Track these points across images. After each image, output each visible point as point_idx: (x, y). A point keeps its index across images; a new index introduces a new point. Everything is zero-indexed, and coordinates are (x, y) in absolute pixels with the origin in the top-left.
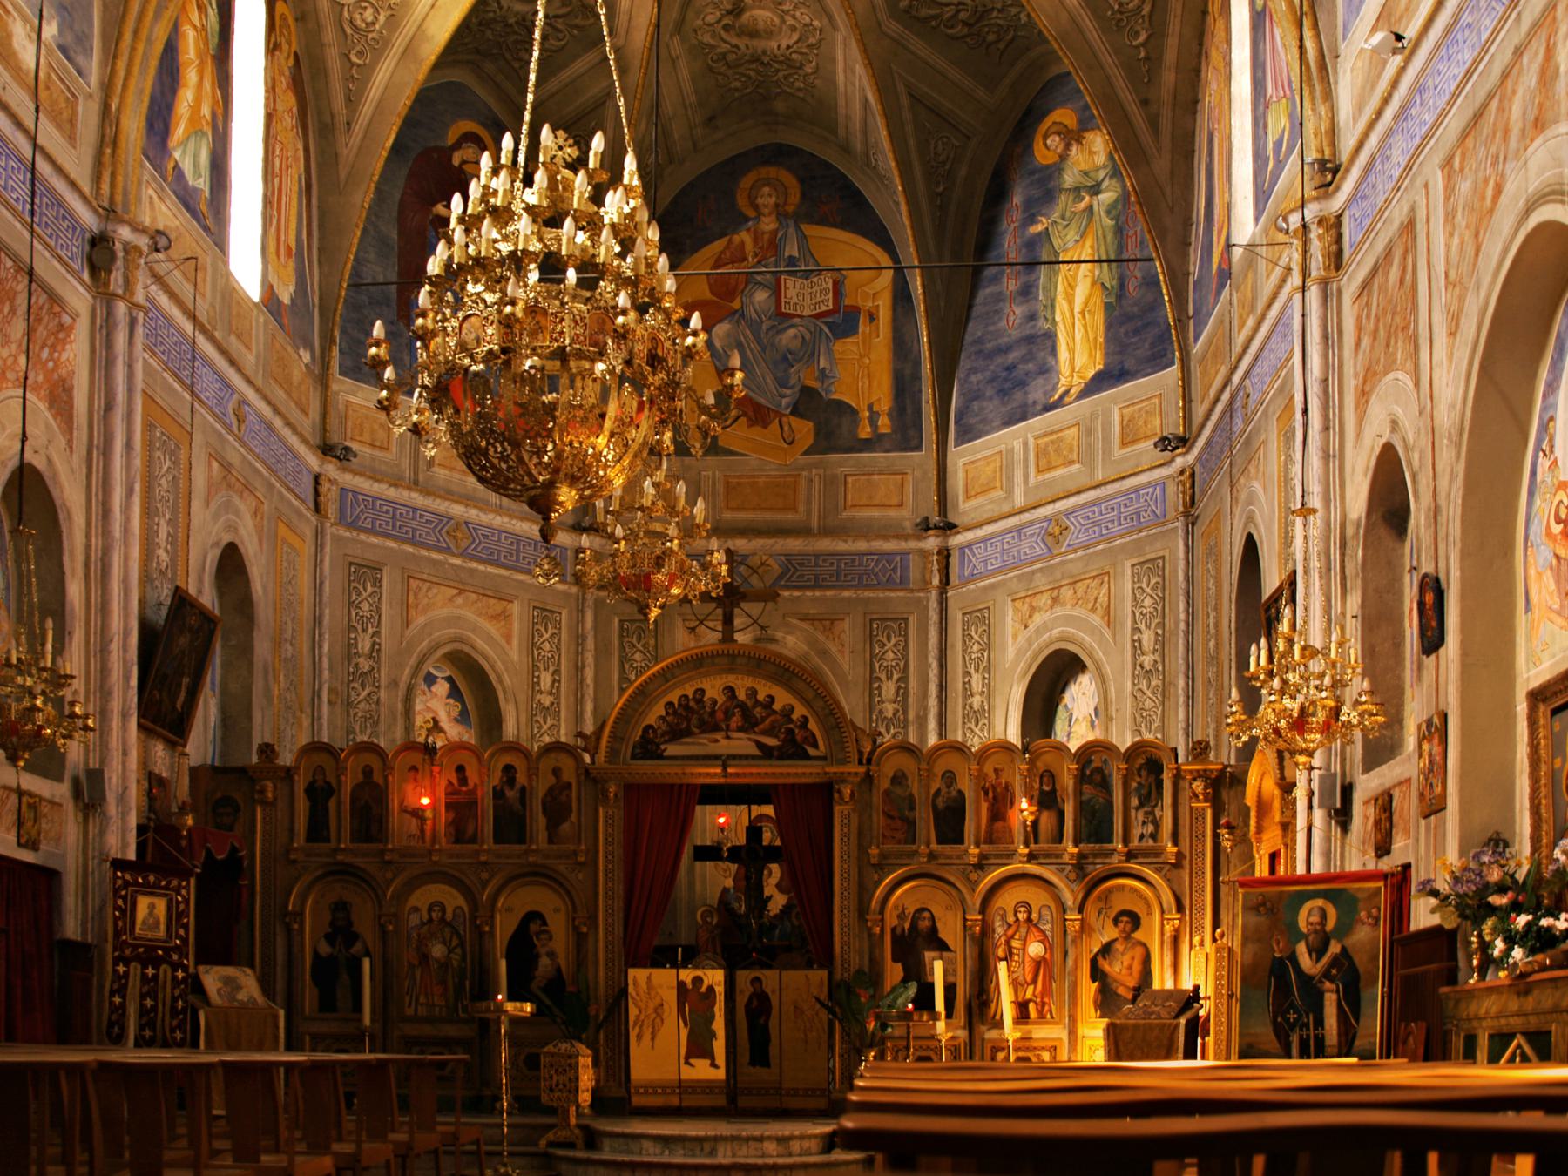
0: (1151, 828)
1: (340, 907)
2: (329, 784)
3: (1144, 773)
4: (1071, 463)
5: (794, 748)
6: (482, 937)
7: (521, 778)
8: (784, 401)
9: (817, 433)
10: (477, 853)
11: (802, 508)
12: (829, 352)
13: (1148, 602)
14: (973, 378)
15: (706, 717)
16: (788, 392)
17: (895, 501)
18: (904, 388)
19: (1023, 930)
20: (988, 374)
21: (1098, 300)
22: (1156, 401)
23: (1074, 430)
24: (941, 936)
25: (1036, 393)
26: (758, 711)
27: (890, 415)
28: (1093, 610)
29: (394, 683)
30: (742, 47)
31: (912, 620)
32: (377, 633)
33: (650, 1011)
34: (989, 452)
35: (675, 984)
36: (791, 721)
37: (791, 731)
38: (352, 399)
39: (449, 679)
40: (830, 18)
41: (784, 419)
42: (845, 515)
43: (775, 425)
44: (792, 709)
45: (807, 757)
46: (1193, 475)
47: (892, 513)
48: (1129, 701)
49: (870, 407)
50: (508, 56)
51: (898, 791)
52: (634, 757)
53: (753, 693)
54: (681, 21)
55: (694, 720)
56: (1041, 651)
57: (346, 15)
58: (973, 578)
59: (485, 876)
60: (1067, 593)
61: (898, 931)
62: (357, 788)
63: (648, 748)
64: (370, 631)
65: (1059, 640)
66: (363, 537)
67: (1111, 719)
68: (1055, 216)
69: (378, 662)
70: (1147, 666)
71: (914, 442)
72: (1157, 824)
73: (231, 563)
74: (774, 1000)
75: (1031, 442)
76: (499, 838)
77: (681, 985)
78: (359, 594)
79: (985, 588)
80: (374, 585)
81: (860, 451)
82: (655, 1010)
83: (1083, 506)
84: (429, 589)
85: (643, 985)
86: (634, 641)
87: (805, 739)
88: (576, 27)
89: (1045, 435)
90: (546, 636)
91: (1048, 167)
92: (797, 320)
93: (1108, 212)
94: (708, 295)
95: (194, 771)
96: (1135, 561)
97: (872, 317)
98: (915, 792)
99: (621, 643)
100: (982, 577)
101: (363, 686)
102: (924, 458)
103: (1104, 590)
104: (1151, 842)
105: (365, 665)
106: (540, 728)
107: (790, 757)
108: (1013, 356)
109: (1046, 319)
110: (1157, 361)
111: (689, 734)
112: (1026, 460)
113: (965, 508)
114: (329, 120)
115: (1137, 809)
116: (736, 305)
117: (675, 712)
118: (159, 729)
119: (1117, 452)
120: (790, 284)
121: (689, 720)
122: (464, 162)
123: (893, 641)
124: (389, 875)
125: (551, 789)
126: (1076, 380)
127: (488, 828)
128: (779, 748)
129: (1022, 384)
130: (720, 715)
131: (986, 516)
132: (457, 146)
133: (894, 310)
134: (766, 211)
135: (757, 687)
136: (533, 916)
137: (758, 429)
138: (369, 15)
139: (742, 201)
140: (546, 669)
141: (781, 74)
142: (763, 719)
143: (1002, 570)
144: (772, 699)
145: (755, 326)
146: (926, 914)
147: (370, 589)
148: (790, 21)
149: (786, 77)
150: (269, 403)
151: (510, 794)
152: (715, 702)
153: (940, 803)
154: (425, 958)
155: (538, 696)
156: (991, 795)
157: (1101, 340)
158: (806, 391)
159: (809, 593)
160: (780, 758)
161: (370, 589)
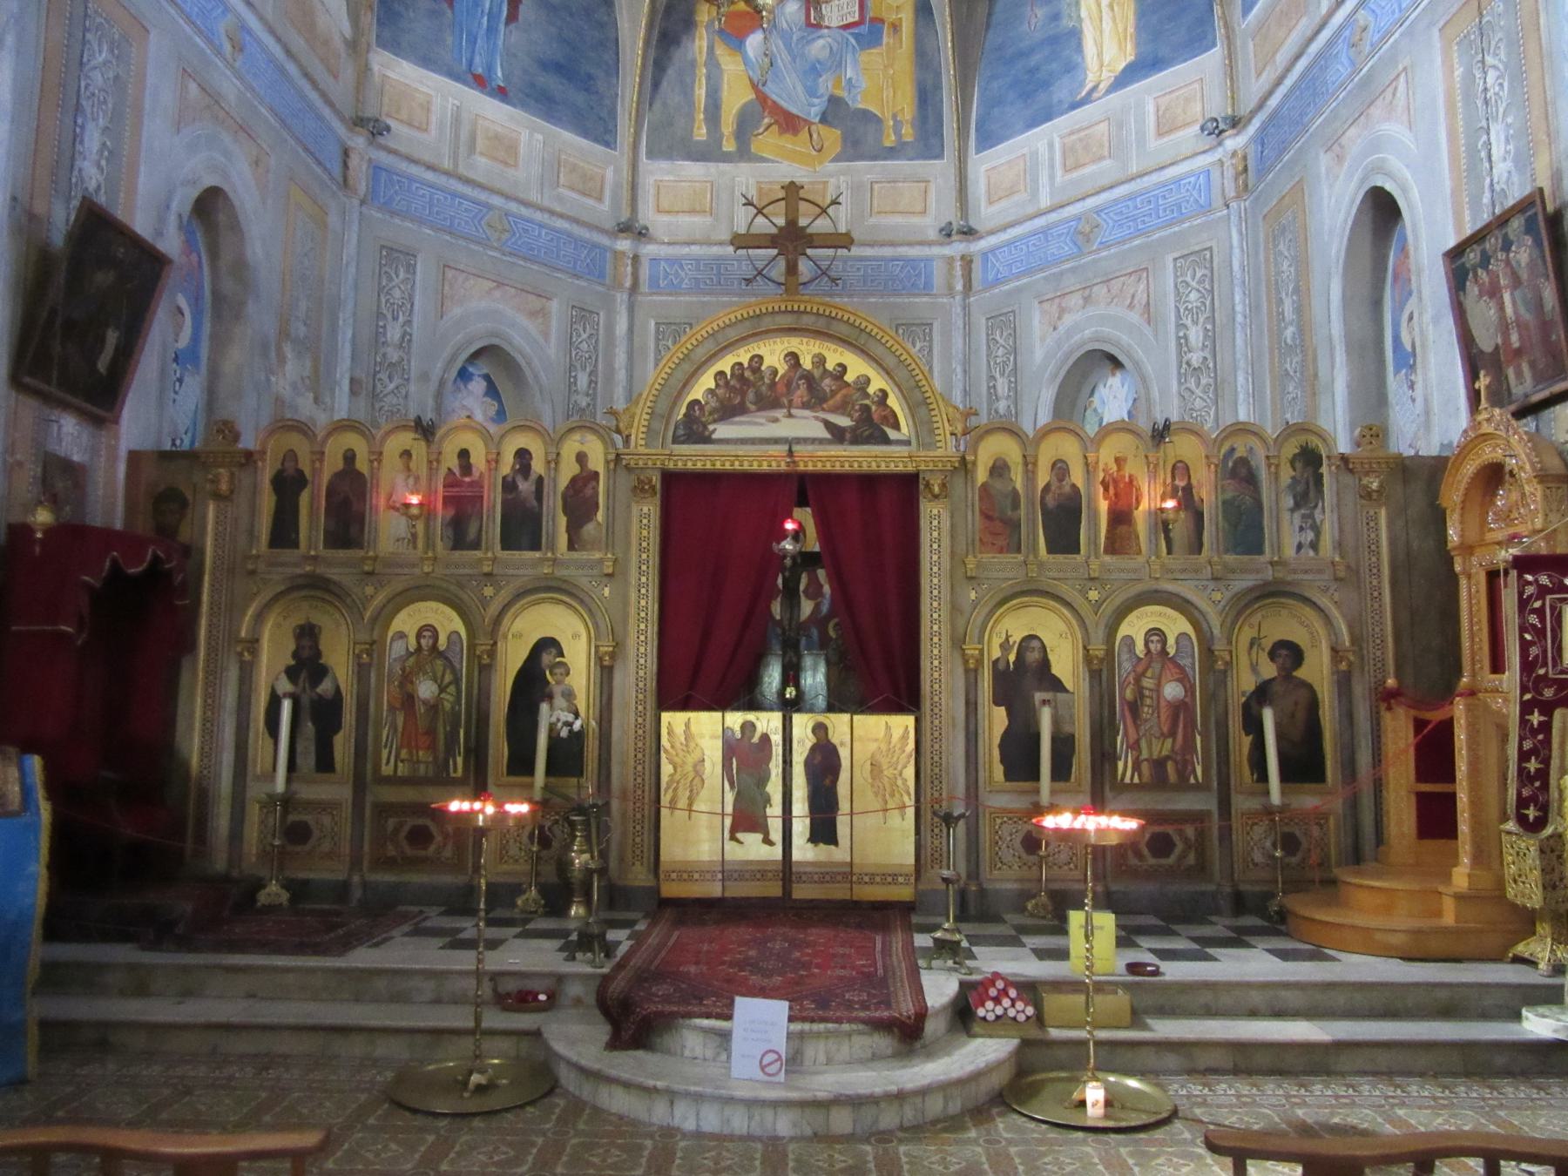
0: (1310, 535)
1: (308, 634)
2: (301, 473)
3: (1298, 465)
4: (1102, 158)
6: (485, 668)
7: (538, 466)
8: (814, 110)
9: (845, 139)
10: (480, 561)
13: (1193, 296)
14: (995, 85)
16: (816, 101)
17: (919, 208)
18: (926, 98)
19: (1157, 666)
22: (1197, 86)
23: (1103, 127)
25: (1060, 92)
26: (827, 384)
27: (913, 125)
28: (1131, 306)
29: (425, 377)
31: (936, 326)
32: (409, 322)
33: (689, 768)
36: (867, 396)
37: (866, 409)
39: (487, 378)
41: (813, 128)
42: (873, 220)
43: (804, 134)
44: (868, 381)
45: (886, 441)
46: (1245, 158)
47: (915, 220)
49: (894, 117)
51: (998, 485)
52: (675, 441)
53: (820, 360)
55: (751, 395)
56: (1071, 352)
58: (998, 282)
59: (488, 591)
60: (1100, 291)
61: (1001, 666)
62: (338, 476)
63: (694, 430)
64: (401, 319)
65: (1091, 340)
69: (408, 353)
70: (1195, 364)
73: (210, 207)
74: (844, 753)
76: (508, 543)
78: (390, 279)
79: (1009, 294)
80: (407, 271)
81: (885, 159)
82: (695, 766)
83: (1116, 201)
84: (467, 279)
85: (679, 729)
87: (885, 419)
89: (1072, 133)
90: (584, 336)
95: (134, 457)
96: (1176, 255)
97: (896, 27)
98: (1019, 486)
99: (657, 346)
100: (1005, 281)
101: (390, 378)
102: (940, 171)
103: (1142, 286)
104: (1311, 553)
105: (394, 355)
108: (1035, 59)
109: (1070, 17)
110: (1197, 41)
111: (741, 410)
112: (1052, 159)
113: (985, 213)
115: (1292, 510)
117: (727, 383)
118: (69, 398)
119: (1153, 143)
121: (743, 394)
123: (918, 345)
124: (369, 590)
125: (574, 480)
126: (1105, 74)
127: (495, 530)
128: (853, 429)
129: (1046, 84)
130: (781, 389)
133: (916, 22)
136: (547, 645)
137: (788, 136)
142: (834, 393)
143: (1028, 272)
145: (786, 37)
146: (1035, 644)
147: (402, 275)
150: (278, 40)
151: (525, 487)
152: (775, 372)
153: (1051, 502)
154: (409, 700)
156: (1112, 491)
157: (1131, 30)
158: (834, 101)
160: (856, 441)
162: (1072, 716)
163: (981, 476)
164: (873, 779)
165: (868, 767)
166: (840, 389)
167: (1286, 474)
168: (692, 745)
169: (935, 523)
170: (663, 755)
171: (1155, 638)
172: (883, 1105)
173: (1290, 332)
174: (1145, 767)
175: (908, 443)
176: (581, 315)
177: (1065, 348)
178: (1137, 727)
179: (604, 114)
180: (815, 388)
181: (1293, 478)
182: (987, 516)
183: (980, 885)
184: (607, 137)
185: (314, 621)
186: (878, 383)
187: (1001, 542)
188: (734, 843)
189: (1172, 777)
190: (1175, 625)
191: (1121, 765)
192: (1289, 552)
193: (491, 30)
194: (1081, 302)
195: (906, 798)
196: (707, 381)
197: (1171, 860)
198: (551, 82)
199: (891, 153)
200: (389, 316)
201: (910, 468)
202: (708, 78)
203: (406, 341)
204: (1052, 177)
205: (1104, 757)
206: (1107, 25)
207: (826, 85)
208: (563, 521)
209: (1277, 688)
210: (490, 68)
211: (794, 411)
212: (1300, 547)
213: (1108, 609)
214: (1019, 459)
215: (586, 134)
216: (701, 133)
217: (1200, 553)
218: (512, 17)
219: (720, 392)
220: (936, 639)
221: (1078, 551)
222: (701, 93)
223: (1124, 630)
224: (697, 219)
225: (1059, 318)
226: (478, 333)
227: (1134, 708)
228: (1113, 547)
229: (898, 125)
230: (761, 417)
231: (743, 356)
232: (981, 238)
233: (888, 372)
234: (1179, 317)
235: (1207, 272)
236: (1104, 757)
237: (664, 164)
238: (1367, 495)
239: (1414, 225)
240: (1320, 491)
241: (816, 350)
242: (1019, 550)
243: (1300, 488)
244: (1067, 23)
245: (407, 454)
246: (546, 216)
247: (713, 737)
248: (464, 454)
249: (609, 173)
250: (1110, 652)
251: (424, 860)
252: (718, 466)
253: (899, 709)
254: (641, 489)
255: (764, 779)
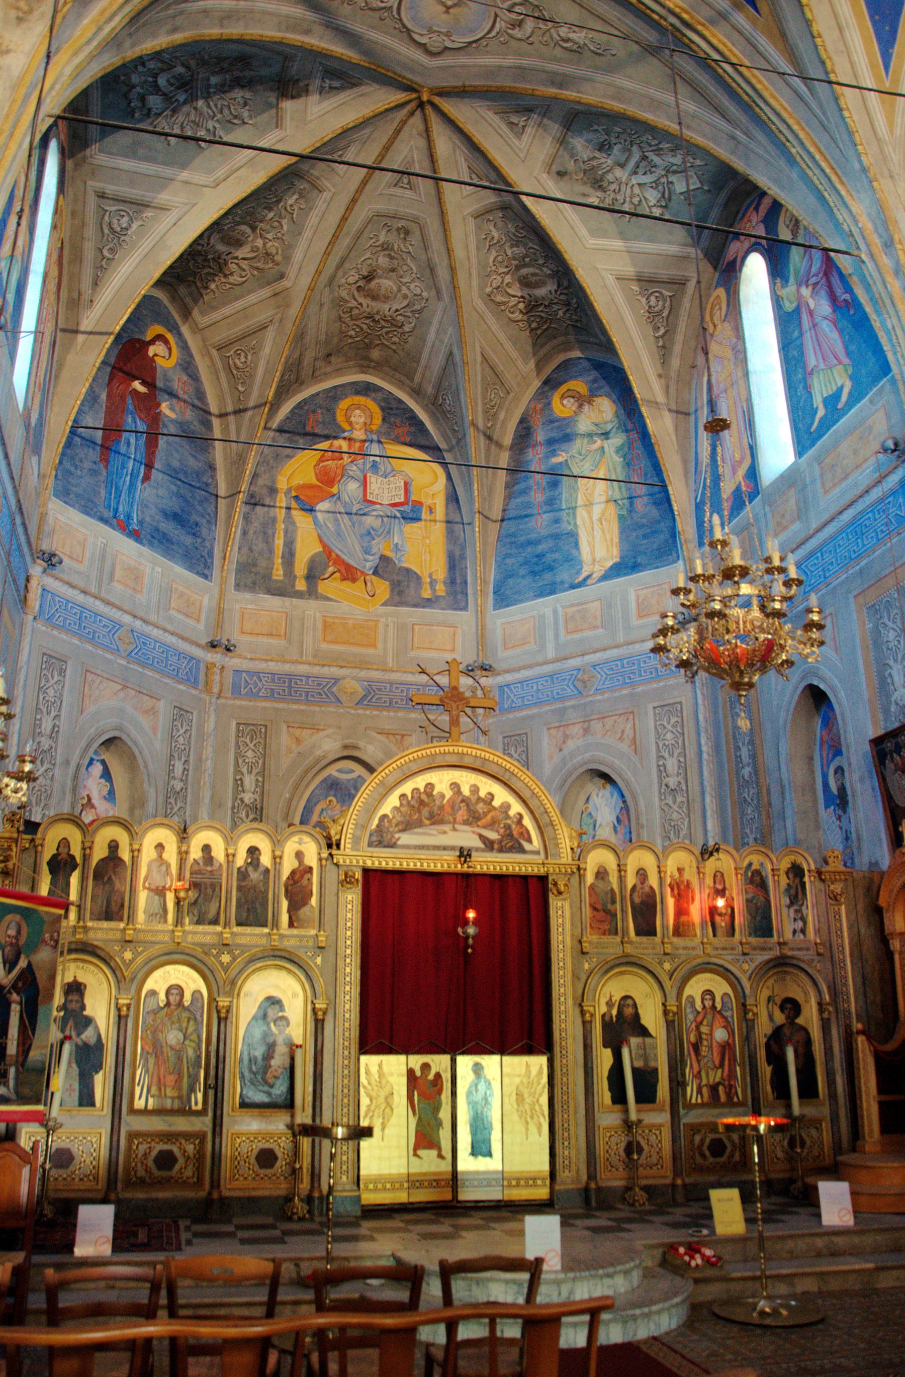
0: (800, 924)
2: (73, 857)
3: (791, 876)
4: (595, 627)
5: (512, 841)
7: (266, 860)
8: (368, 564)
11: (380, 645)
12: (401, 531)
13: (669, 736)
14: (508, 561)
15: (435, 809)
16: (371, 558)
17: (449, 647)
18: (454, 564)
19: (709, 1017)
20: (521, 559)
21: (612, 511)
23: (597, 604)
24: (643, 1022)
25: (563, 575)
27: (445, 583)
30: (365, 306)
33: (382, 1100)
34: (523, 616)
35: (405, 1072)
37: (508, 827)
38: (59, 516)
39: (103, 762)
40: (438, 292)
43: (360, 583)
45: (522, 850)
48: (658, 813)
49: (430, 576)
50: (199, 284)
51: (601, 884)
53: (475, 789)
54: (333, 277)
57: (106, 218)
60: (596, 726)
61: (607, 1018)
66: (55, 632)
67: (642, 826)
68: (574, 452)
70: (672, 785)
71: (463, 604)
72: (804, 920)
75: (560, 610)
77: (410, 1073)
81: (424, 607)
82: (386, 1098)
85: (374, 1069)
86: (248, 741)
88: (257, 269)
89: (572, 606)
90: (182, 731)
91: (565, 419)
92: (378, 506)
93: (617, 452)
94: (314, 481)
96: (656, 704)
100: (519, 709)
102: (465, 619)
104: (802, 936)
106: (172, 809)
107: (510, 850)
108: (541, 548)
109: (568, 522)
111: (420, 824)
112: (556, 623)
114: (76, 295)
115: (789, 907)
116: (335, 490)
120: (373, 480)
121: (420, 812)
122: (156, 355)
125: (293, 873)
128: (501, 841)
131: (521, 664)
132: (152, 342)
134: (357, 427)
135: (479, 785)
137: (347, 583)
138: (124, 222)
139: (340, 418)
140: (180, 759)
141: (385, 330)
142: (485, 814)
144: (492, 796)
146: (630, 1002)
147: (56, 678)
148: (404, 290)
149: (387, 333)
151: (254, 876)
152: (443, 796)
153: (637, 900)
155: (172, 782)
156: (676, 891)
157: (616, 540)
158: (384, 558)
159: (385, 713)
160: (501, 850)
161: (56, 678)
162: (656, 1055)
163: (590, 878)
164: (518, 1105)
165: (514, 1097)
166: (489, 811)
167: (784, 881)
168: (384, 1082)
169: (560, 912)
170: (362, 1090)
171: (708, 997)
172: (639, 1321)
173: (746, 771)
174: (705, 1090)
175: (538, 853)
176: (181, 713)
177: (569, 765)
178: (699, 1061)
179: (205, 554)
180: (474, 811)
181: (788, 885)
182: (594, 909)
183: (597, 1184)
184: (206, 572)
185: (80, 980)
186: (516, 808)
187: (606, 926)
188: (416, 1159)
189: (723, 1098)
190: (721, 987)
191: (689, 1089)
192: (788, 935)
193: (132, 485)
194: (581, 732)
195: (542, 1119)
196: (393, 801)
197: (724, 1159)
198: (168, 527)
199: (428, 603)
200: (45, 710)
201: (542, 871)
202: (286, 532)
203: (54, 732)
204: (557, 636)
205: (677, 1084)
206: (598, 534)
207: (380, 547)
208: (285, 904)
209: (787, 1031)
210: (129, 516)
211: (457, 826)
212: (795, 932)
213: (678, 975)
214: (615, 867)
215: (191, 568)
216: (278, 573)
217: (733, 935)
218: (147, 478)
219: (403, 809)
220: (562, 999)
221: (655, 934)
222: (279, 542)
223: (687, 991)
224: (274, 641)
225: (564, 742)
226: (107, 726)
227: (696, 1047)
228: (677, 932)
229: (433, 583)
230: (434, 829)
231: (420, 782)
232: (499, 674)
233: (524, 802)
234: (658, 750)
235: (679, 720)
236: (677, 1084)
237: (248, 596)
238: (835, 898)
239: (842, 714)
240: (805, 894)
241: (473, 782)
242: (616, 933)
243: (793, 892)
244: (566, 527)
245: (160, 847)
246: (161, 632)
247: (399, 1075)
248: (207, 848)
249: (206, 600)
250: (679, 1007)
251: (169, 1180)
252: (405, 865)
253: (529, 1050)
254: (347, 880)
255: (437, 1109)
